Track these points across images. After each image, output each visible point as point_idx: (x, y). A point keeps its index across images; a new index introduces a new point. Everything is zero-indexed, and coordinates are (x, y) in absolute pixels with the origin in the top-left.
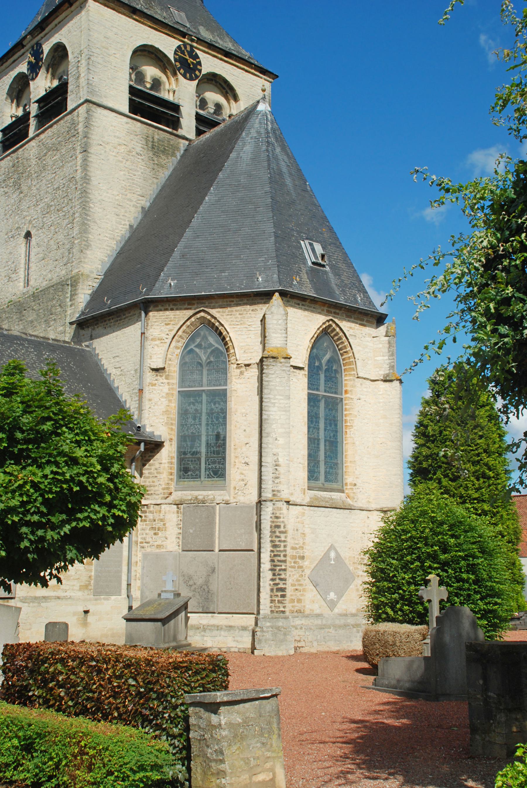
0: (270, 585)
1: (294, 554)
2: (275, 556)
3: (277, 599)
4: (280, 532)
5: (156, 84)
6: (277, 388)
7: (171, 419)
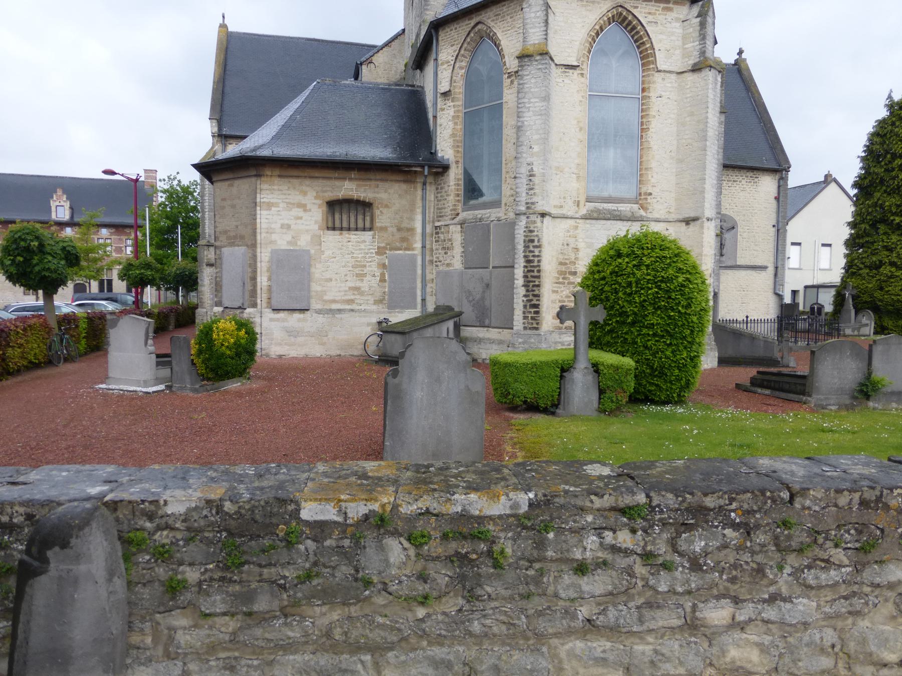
2: (528, 271)
4: (534, 247)
6: (532, 90)
7: (458, 141)
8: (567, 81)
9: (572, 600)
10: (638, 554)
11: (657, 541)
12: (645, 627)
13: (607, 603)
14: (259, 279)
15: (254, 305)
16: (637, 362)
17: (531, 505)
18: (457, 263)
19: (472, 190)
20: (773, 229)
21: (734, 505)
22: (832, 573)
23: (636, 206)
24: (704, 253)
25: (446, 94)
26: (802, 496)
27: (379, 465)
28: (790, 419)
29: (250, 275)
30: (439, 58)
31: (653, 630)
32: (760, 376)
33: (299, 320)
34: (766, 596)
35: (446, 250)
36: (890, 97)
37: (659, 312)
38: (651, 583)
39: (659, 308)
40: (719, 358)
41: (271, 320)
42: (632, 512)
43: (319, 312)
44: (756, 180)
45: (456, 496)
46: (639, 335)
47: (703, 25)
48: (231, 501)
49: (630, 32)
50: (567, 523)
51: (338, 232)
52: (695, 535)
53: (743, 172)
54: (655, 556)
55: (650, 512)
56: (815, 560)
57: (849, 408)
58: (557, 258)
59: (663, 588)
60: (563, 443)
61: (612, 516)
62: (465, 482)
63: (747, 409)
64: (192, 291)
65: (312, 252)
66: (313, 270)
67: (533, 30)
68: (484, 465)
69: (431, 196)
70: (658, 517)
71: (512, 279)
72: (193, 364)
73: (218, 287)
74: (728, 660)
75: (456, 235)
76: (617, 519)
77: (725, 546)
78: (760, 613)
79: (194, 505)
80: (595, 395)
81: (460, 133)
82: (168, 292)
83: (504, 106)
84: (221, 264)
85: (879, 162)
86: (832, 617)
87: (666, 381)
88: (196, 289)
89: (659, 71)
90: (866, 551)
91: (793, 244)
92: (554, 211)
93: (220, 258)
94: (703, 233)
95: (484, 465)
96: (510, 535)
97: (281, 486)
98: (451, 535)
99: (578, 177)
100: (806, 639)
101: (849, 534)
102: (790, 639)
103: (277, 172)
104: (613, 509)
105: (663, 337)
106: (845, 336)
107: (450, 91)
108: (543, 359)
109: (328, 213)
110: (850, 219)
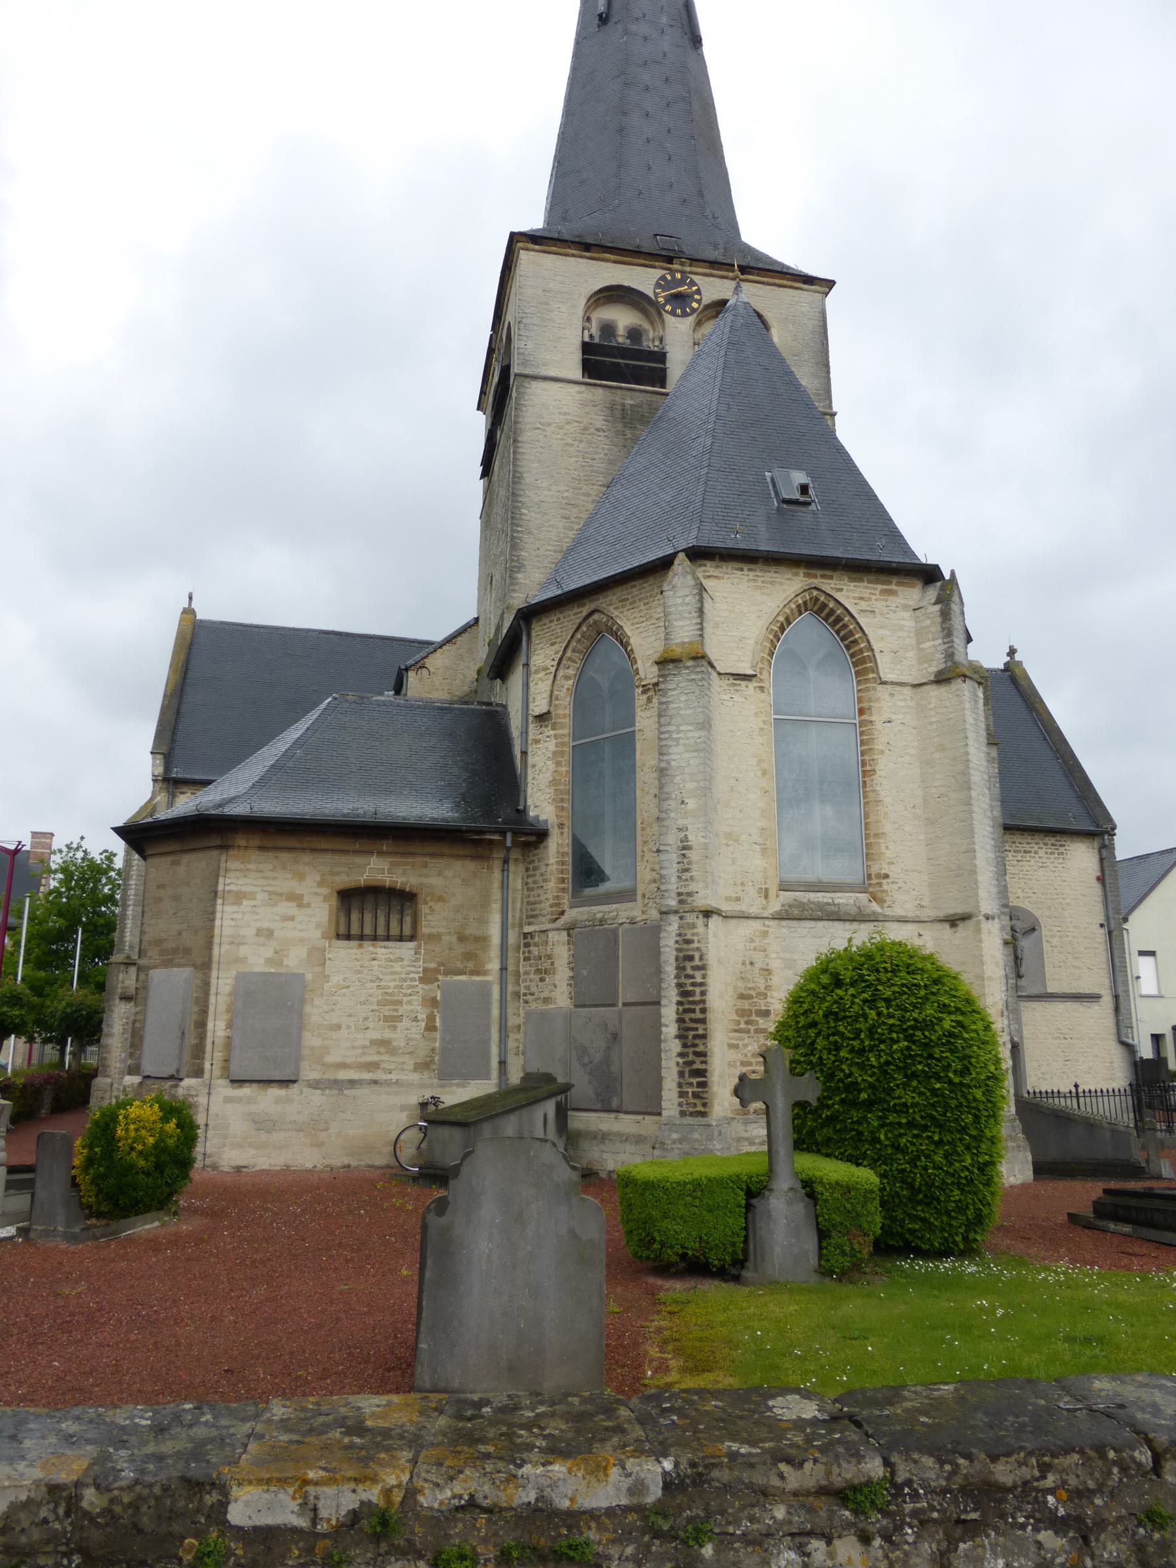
0: (678, 1064)
1: (747, 1007)
2: (686, 1011)
3: (690, 1090)
5: (635, 334)
8: (736, 698)
14: (210, 1026)
15: (198, 1073)
16: (883, 1176)
17: (667, 1486)
18: (562, 998)
19: (586, 872)
20: (1102, 931)
21: (1050, 1480)
23: (863, 897)
25: (542, 718)
27: (389, 1403)
29: (195, 1017)
30: (532, 663)
32: (1109, 1199)
33: (278, 1101)
35: (543, 973)
37: (914, 1083)
39: (914, 1075)
40: (1035, 1164)
41: (227, 1100)
42: (860, 1498)
43: (315, 1085)
44: (1062, 849)
45: (527, 1469)
46: (882, 1126)
47: (945, 615)
48: (98, 1487)
49: (833, 625)
51: (354, 943)
52: (983, 1546)
53: (1037, 837)
58: (735, 988)
60: (753, 1336)
62: (545, 1437)
63: (1092, 1265)
64: (91, 1043)
65: (309, 977)
66: (308, 1009)
67: (681, 623)
68: (584, 1401)
69: (516, 881)
70: (908, 1507)
71: (657, 1025)
72: (74, 1184)
73: (136, 1039)
75: (560, 949)
76: (832, 1513)
79: (23, 1497)
80: (810, 1242)
81: (566, 779)
82: (49, 1047)
83: (638, 736)
84: (146, 998)
87: (939, 1212)
88: (98, 1041)
89: (885, 683)
91: (1142, 953)
92: (725, 907)
93: (146, 988)
94: (981, 941)
95: (584, 1401)
96: (629, 1550)
97: (197, 1452)
98: (515, 1554)
99: (764, 851)
103: (256, 841)
104: (823, 1491)
105: (925, 1128)
107: (549, 712)
108: (713, 1172)
109: (338, 910)
110: (920, 585)
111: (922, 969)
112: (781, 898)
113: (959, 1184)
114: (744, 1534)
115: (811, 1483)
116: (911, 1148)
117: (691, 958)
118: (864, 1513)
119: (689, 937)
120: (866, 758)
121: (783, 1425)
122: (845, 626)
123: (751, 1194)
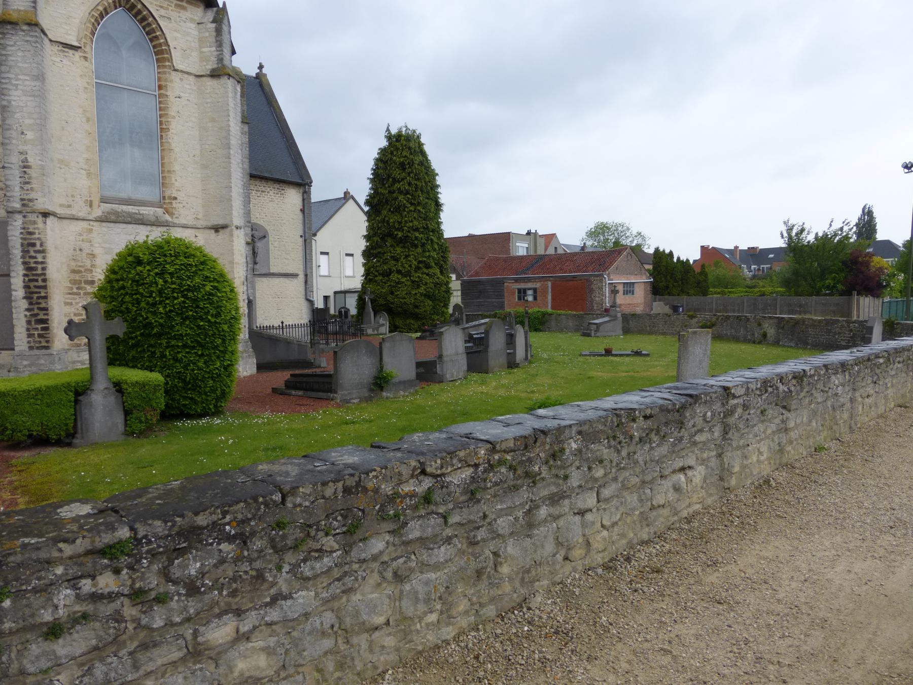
1: (77, 278)
2: (30, 280)
4: (36, 252)
6: (20, 65)
8: (65, 61)
9: (45, 672)
10: (126, 595)
11: (147, 575)
12: (141, 672)
13: (92, 660)
21: (228, 518)
22: (326, 560)
23: (160, 211)
24: (236, 260)
26: (292, 495)
28: (320, 416)
31: (152, 672)
32: (293, 379)
34: (268, 600)
36: (388, 130)
37: (187, 322)
38: (143, 622)
39: (187, 318)
46: (167, 347)
47: (219, 31)
50: (28, 582)
52: (189, 559)
53: (270, 183)
54: (146, 592)
55: (136, 546)
56: (310, 552)
57: (368, 399)
58: (68, 265)
59: (158, 623)
60: (79, 477)
61: (89, 561)
70: (145, 549)
71: (8, 290)
74: (236, 674)
76: (95, 563)
77: (222, 561)
78: (263, 618)
80: (119, 418)
85: (384, 185)
86: (329, 601)
87: (200, 393)
90: (352, 533)
91: (322, 253)
92: (60, 211)
94: (233, 241)
99: (89, 175)
100: (308, 628)
101: (337, 521)
102: (295, 634)
104: (89, 553)
105: (194, 348)
106: (367, 335)
108: (51, 383)
110: (365, 233)
111: (193, 255)
112: (102, 208)
113: (212, 377)
114: (33, 588)
115: (81, 550)
116: (185, 359)
117: (34, 245)
118: (116, 558)
119: (31, 230)
120: (163, 120)
121: (65, 521)
122: (149, 25)
123: (78, 394)
